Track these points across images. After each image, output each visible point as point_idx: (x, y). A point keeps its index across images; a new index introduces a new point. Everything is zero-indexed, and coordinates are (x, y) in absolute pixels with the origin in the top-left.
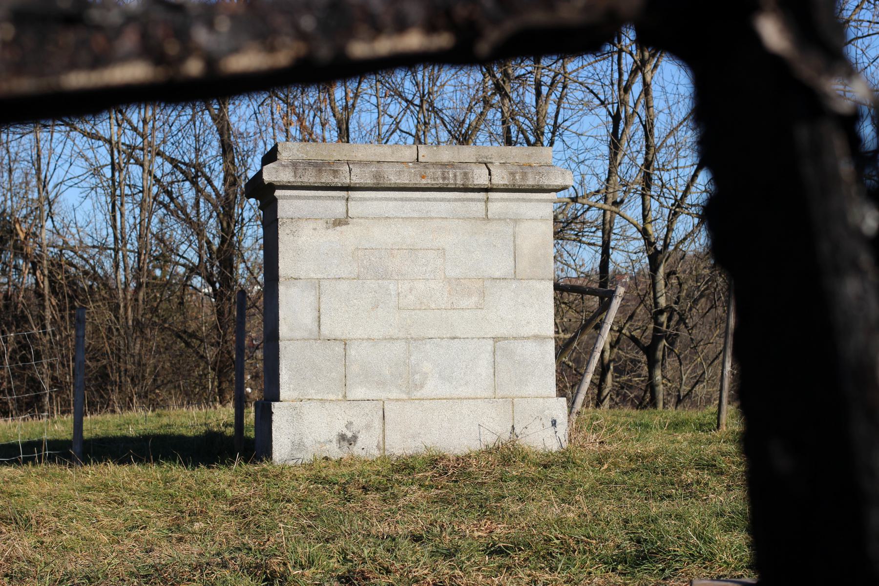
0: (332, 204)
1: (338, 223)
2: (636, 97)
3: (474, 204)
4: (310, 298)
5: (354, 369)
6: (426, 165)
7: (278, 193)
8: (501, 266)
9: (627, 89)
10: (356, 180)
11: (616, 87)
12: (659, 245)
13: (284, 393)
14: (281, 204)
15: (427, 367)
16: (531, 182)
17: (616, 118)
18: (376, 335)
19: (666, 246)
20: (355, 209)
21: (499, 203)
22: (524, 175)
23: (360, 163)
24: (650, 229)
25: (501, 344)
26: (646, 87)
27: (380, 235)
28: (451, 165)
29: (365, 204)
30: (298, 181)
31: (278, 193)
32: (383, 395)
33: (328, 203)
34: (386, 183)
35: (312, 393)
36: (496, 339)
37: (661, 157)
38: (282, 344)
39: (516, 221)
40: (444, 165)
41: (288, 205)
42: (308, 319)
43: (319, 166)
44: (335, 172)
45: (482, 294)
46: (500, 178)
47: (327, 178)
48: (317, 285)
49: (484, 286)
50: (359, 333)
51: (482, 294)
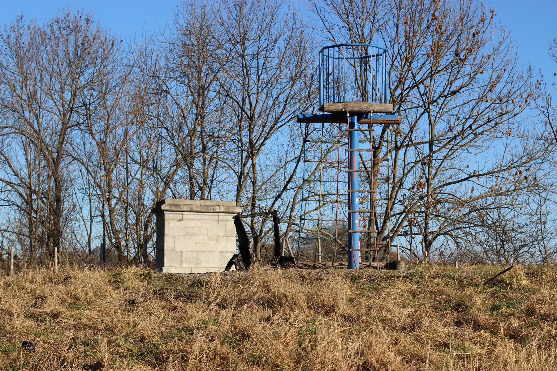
0: (179, 216)
1: (180, 220)
2: (249, 167)
3: (215, 216)
4: (172, 240)
5: (184, 259)
6: (203, 206)
7: (165, 212)
8: (222, 233)
9: (245, 165)
10: (185, 209)
11: (240, 163)
12: (258, 233)
13: (165, 265)
14: (165, 215)
15: (202, 259)
16: (230, 211)
17: (240, 177)
18: (189, 250)
19: (261, 233)
20: (184, 217)
21: (222, 216)
22: (229, 209)
23: (186, 205)
24: (255, 226)
25: (222, 254)
26: (253, 165)
27: (191, 224)
28: (210, 206)
29: (187, 216)
30: (171, 209)
31: (165, 212)
32: (191, 266)
33: (170, 215)
34: (193, 210)
35: (173, 265)
36: (221, 252)
37: (259, 194)
38: (165, 252)
39: (226, 221)
40: (208, 206)
41: (167, 216)
42: (172, 245)
43: (176, 206)
44: (180, 207)
45: (217, 240)
46: (222, 210)
47: (178, 209)
48: (174, 237)
49: (218, 238)
50: (185, 250)
51: (217, 240)
